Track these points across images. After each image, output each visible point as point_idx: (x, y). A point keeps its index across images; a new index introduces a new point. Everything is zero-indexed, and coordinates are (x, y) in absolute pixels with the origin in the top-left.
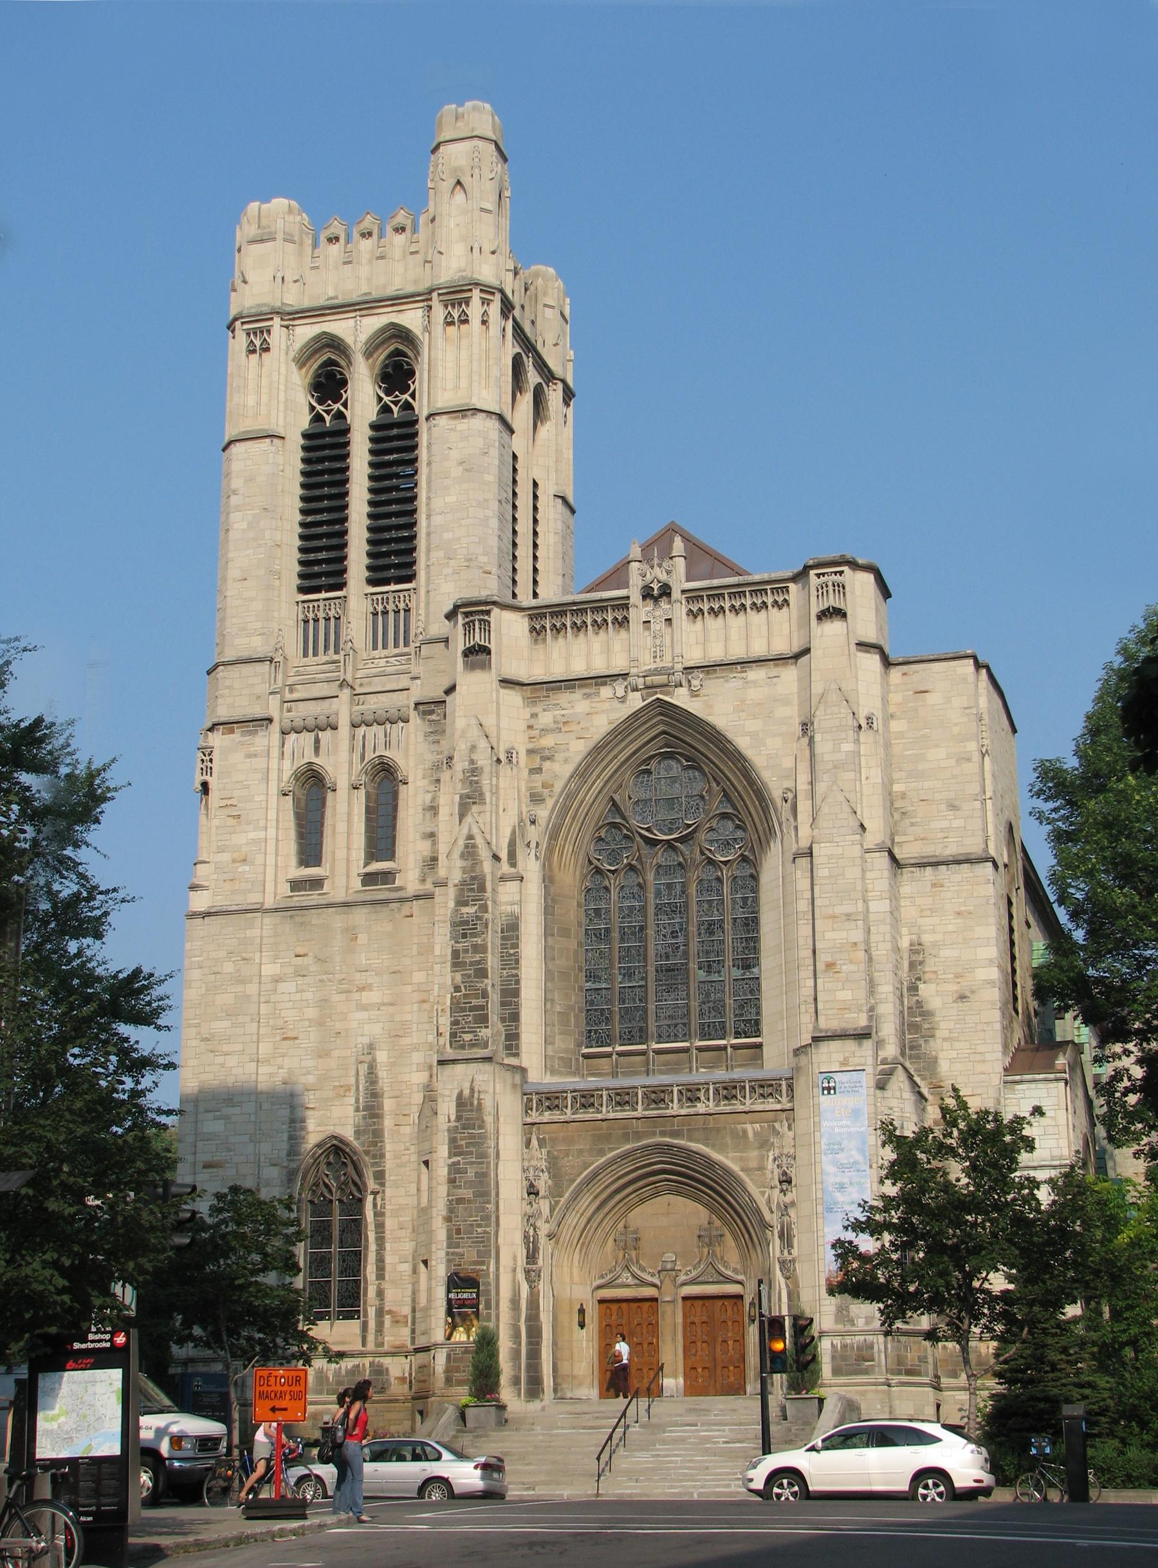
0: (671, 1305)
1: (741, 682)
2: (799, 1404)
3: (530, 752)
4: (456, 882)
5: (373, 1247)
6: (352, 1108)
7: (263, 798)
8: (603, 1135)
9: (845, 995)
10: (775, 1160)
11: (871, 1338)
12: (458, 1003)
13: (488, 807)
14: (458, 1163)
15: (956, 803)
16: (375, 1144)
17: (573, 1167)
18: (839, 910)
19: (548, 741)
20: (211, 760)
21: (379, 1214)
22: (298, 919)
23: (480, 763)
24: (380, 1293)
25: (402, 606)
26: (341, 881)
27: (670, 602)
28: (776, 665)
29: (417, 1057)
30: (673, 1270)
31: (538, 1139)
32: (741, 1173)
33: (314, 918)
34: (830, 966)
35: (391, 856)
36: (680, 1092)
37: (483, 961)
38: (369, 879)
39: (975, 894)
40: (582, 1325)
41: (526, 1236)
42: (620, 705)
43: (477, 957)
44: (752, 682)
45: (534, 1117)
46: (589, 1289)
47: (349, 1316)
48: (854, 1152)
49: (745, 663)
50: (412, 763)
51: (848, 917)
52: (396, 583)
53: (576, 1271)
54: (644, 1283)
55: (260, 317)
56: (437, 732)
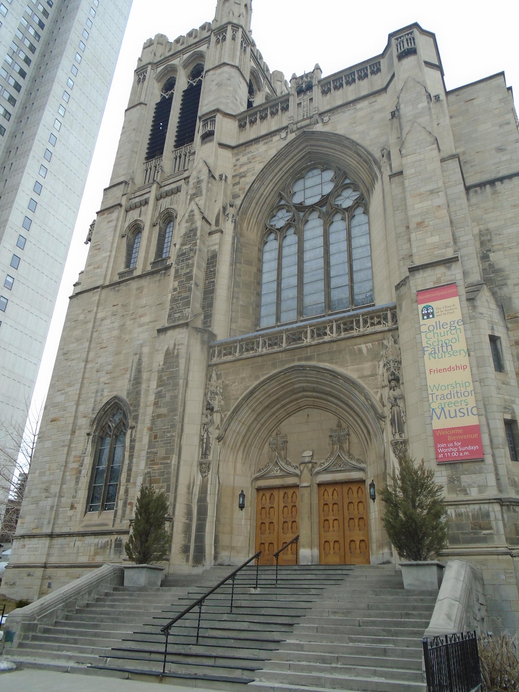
0: (308, 490)
2: (414, 570)
3: (234, 177)
6: (127, 380)
9: (436, 239)
10: (384, 366)
11: (486, 506)
15: (503, 147)
18: (423, 190)
21: (132, 441)
22: (117, 289)
31: (217, 374)
34: (419, 225)
36: (312, 332)
40: (242, 507)
43: (188, 270)
44: (359, 109)
45: (215, 360)
46: (249, 480)
47: (104, 508)
51: (432, 192)
53: (239, 466)
54: (289, 475)
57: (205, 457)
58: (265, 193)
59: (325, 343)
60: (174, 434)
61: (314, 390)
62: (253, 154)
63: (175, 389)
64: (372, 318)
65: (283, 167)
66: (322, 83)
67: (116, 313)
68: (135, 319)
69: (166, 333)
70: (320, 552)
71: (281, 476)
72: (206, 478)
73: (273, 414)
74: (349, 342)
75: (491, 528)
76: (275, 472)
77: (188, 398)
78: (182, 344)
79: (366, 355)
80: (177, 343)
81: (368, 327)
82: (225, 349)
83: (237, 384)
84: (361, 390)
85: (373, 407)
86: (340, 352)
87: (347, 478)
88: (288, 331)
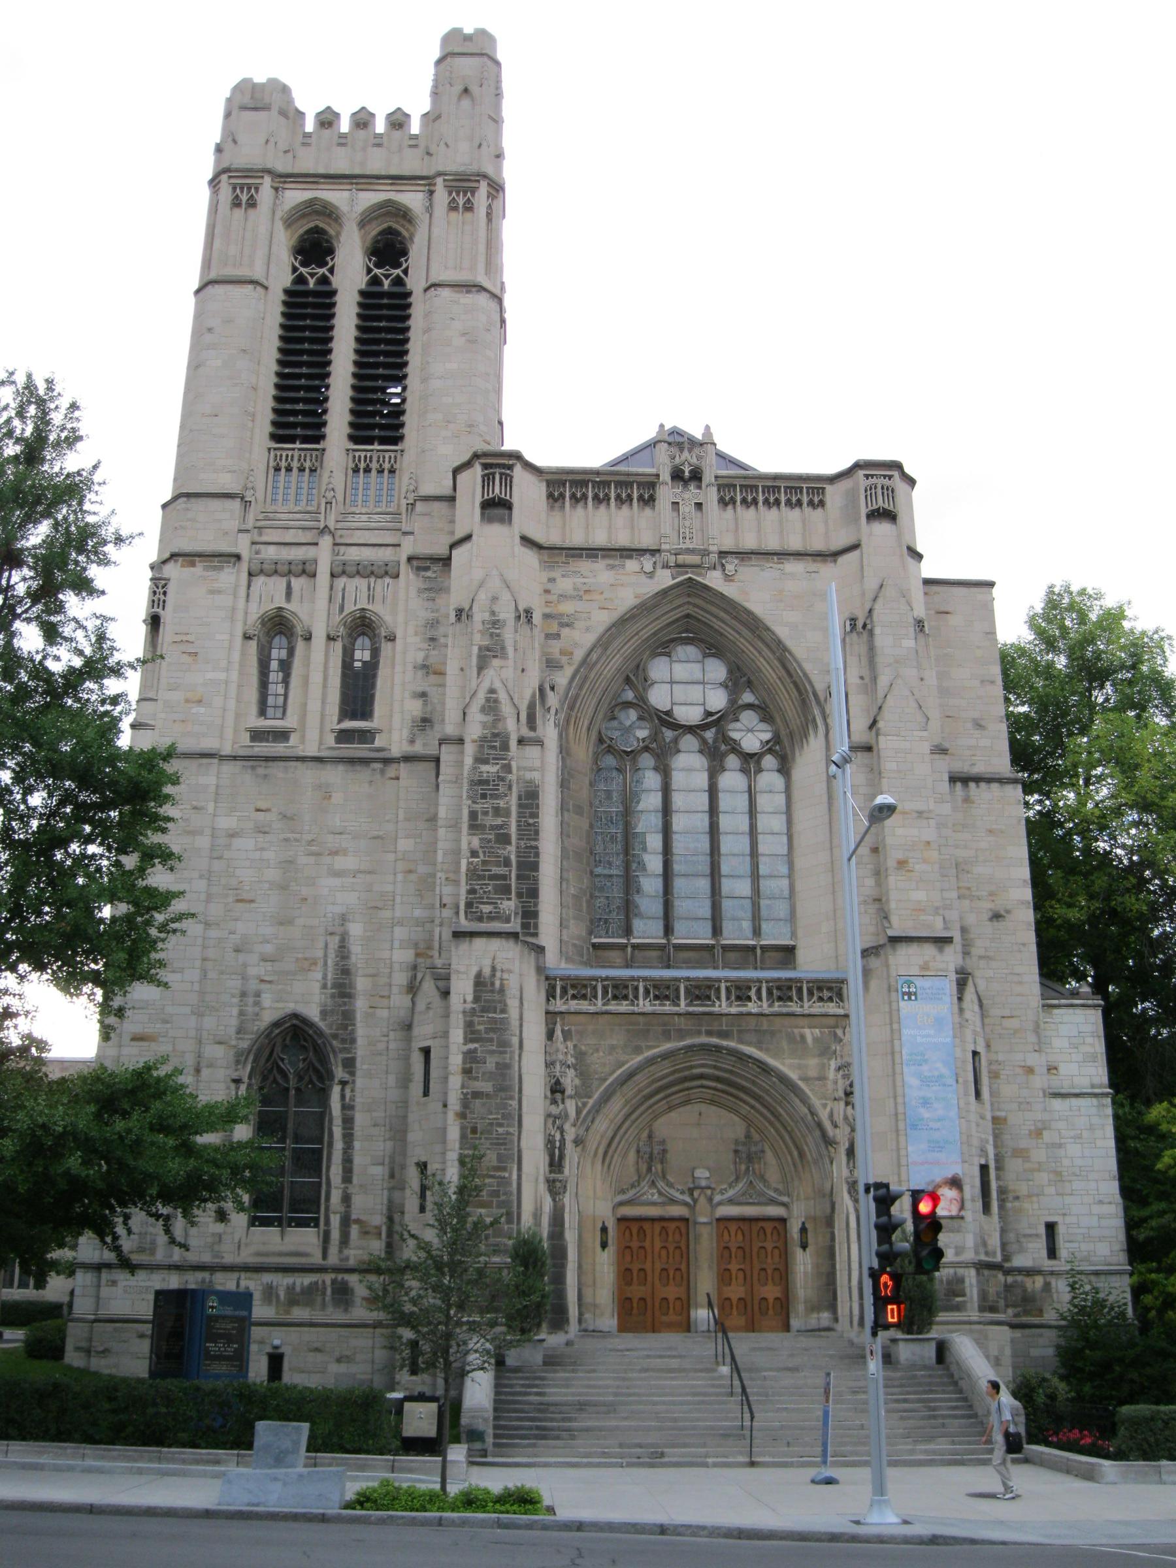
3: (547, 616)
4: (475, 737)
5: (338, 1145)
6: (318, 985)
7: (226, 637)
8: (641, 1028)
9: (920, 895)
12: (475, 870)
13: (510, 662)
15: (982, 723)
16: (345, 1027)
17: (604, 1065)
19: (567, 608)
20: (165, 593)
21: (347, 1107)
22: (261, 771)
23: (502, 616)
24: (346, 1199)
25: (387, 466)
26: (313, 734)
27: (699, 487)
28: (814, 561)
29: (400, 933)
30: (709, 1188)
31: (563, 1031)
32: (800, 1083)
33: (276, 769)
34: (902, 864)
35: (366, 714)
36: (727, 988)
38: (344, 736)
40: (604, 1245)
42: (648, 580)
43: (499, 821)
45: (559, 1005)
46: (610, 1205)
48: (939, 1065)
49: (783, 555)
50: (401, 618)
52: (380, 444)
53: (599, 1183)
54: (673, 1201)
55: (248, 172)
56: (434, 590)
59: (750, 1014)
61: (718, 1079)
62: (585, 580)
63: (505, 1052)
64: (820, 989)
66: (721, 481)
67: (267, 829)
68: (318, 854)
69: (471, 942)
70: (788, 1322)
73: (650, 1107)
74: (787, 1021)
75: (964, 1295)
77: (524, 1071)
78: (510, 971)
80: (498, 967)
82: (573, 986)
83: (601, 1054)
84: (804, 1100)
85: (820, 1125)
86: (773, 1033)
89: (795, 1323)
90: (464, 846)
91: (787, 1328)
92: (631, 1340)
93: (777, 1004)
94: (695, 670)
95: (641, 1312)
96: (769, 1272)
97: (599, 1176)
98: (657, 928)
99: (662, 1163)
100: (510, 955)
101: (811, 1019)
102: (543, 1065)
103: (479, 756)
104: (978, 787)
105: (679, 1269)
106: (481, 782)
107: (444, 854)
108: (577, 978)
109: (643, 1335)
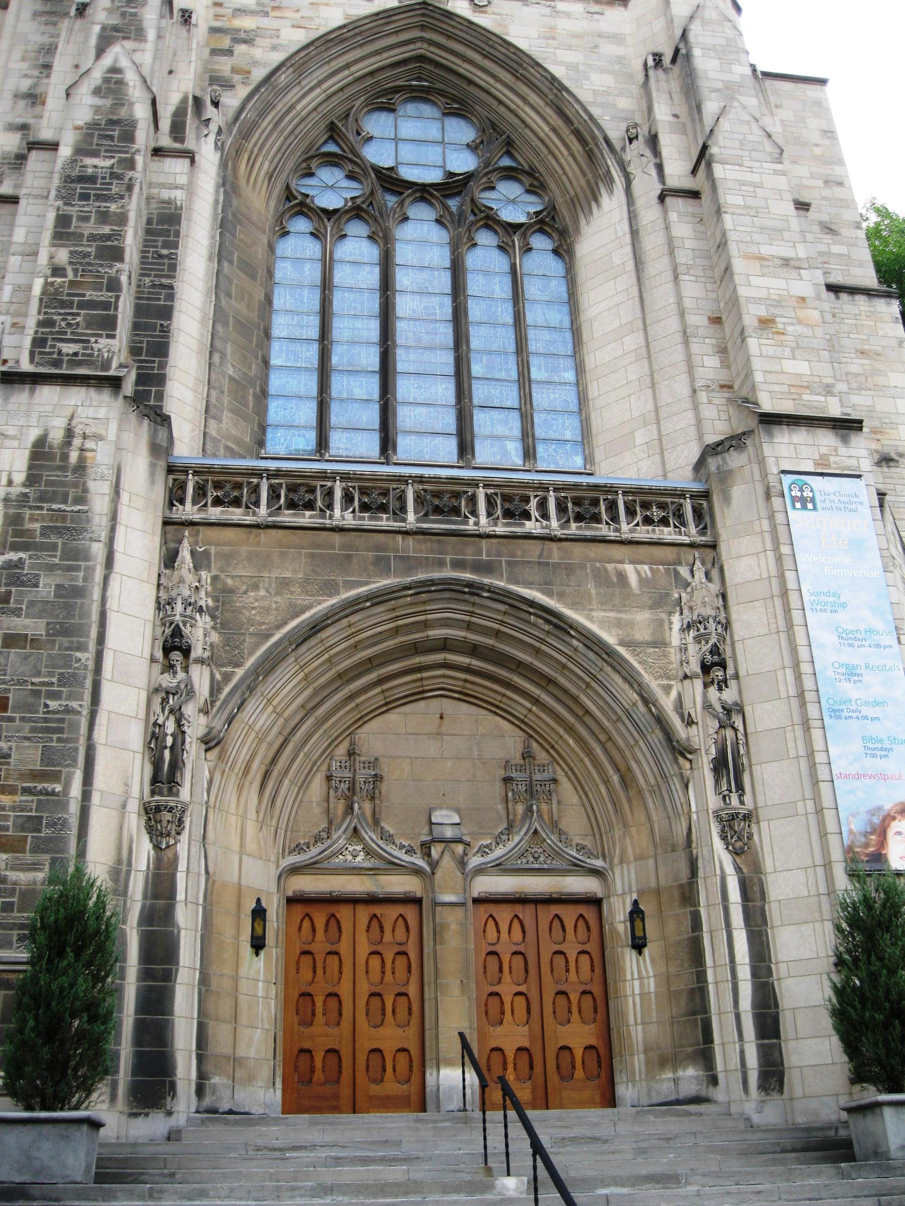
1: (547, 11)
3: (214, 30)
4: (80, 123)
9: (800, 367)
12: (57, 292)
14: (20, 563)
15: (833, 227)
17: (268, 610)
18: (766, 250)
19: (246, 23)
30: (459, 841)
31: (193, 553)
32: (621, 650)
34: (765, 323)
36: (489, 499)
37: (117, 235)
39: (881, 333)
40: (258, 944)
41: (155, 737)
43: (106, 230)
45: (188, 510)
46: (273, 872)
53: (251, 828)
54: (394, 866)
57: (170, 790)
58: (299, 107)
59: (529, 537)
60: (74, 704)
61: (474, 650)
63: (77, 568)
64: (646, 506)
65: (356, 62)
69: (32, 391)
71: (370, 869)
72: (169, 853)
73: (351, 697)
76: (350, 858)
78: (98, 438)
79: (637, 592)
80: (78, 430)
81: (637, 525)
82: (218, 486)
83: (262, 592)
84: (631, 678)
85: (660, 721)
86: (570, 569)
87: (554, 890)
88: (421, 482)
89: (625, 1091)
90: (43, 259)
91: (610, 1100)
92: (306, 1128)
93: (574, 525)
94: (433, 130)
95: (323, 1076)
96: (574, 998)
97: (252, 814)
98: (369, 445)
99: (373, 798)
100: (102, 413)
101: (634, 548)
102: (152, 605)
103: (84, 146)
104: (838, 298)
105: (405, 953)
106: (82, 179)
107: (14, 291)
108: (225, 471)
109: (331, 1117)
